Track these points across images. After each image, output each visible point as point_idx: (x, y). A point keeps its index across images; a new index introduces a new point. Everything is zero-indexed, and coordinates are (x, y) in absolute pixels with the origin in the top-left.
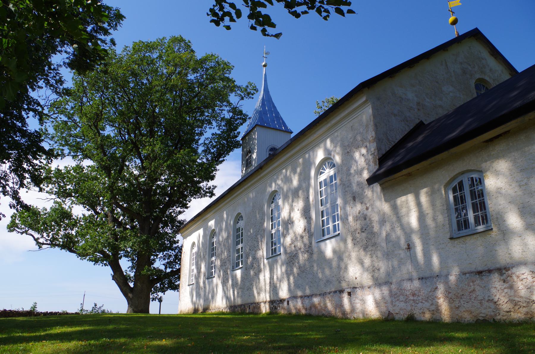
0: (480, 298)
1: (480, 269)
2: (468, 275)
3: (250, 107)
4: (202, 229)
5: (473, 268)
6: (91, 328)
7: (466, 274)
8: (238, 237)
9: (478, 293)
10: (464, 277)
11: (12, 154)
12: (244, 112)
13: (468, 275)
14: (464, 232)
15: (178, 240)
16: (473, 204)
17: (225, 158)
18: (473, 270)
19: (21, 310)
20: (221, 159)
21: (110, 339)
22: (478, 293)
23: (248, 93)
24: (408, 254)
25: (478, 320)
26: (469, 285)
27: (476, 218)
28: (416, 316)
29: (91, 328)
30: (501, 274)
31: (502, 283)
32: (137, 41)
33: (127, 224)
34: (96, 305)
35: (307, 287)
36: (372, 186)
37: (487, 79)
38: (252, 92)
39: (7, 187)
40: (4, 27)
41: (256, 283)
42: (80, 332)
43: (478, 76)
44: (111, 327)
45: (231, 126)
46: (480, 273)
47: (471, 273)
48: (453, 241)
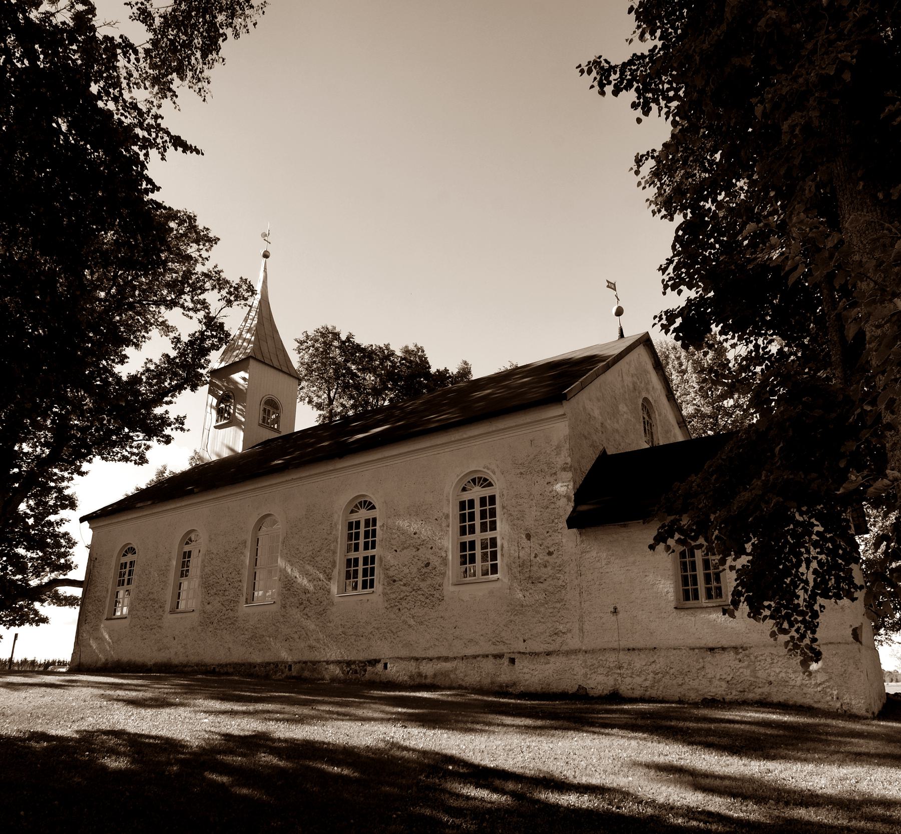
0: (709, 676)
1: (711, 645)
2: (697, 651)
3: (236, 319)
4: (233, 376)
5: (702, 643)
6: (421, 711)
7: (693, 649)
8: (122, 575)
9: (707, 671)
10: (691, 652)
11: (717, 326)
12: (226, 329)
13: (697, 651)
14: (692, 603)
15: (856, 599)
16: (496, 547)
17: (174, 400)
18: (702, 645)
19: (503, 369)
20: (166, 399)
21: (741, 552)
22: (707, 671)
23: (236, 293)
24: (663, 653)
25: (807, 808)
26: (697, 661)
27: (356, 564)
28: (621, 692)
29: (421, 711)
30: (737, 653)
31: (737, 662)
32: (411, 347)
33: (862, 276)
34: (639, 121)
35: (289, 765)
36: (598, 453)
37: (650, 399)
38: (246, 295)
39: (805, 690)
40: (45, 421)
41: (186, 693)
42: (533, 707)
43: (644, 395)
44: (713, 726)
45: (197, 348)
46: (712, 649)
47: (700, 648)
48: (678, 611)
